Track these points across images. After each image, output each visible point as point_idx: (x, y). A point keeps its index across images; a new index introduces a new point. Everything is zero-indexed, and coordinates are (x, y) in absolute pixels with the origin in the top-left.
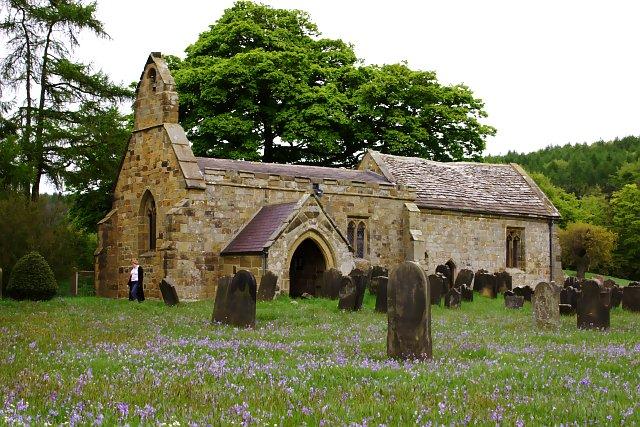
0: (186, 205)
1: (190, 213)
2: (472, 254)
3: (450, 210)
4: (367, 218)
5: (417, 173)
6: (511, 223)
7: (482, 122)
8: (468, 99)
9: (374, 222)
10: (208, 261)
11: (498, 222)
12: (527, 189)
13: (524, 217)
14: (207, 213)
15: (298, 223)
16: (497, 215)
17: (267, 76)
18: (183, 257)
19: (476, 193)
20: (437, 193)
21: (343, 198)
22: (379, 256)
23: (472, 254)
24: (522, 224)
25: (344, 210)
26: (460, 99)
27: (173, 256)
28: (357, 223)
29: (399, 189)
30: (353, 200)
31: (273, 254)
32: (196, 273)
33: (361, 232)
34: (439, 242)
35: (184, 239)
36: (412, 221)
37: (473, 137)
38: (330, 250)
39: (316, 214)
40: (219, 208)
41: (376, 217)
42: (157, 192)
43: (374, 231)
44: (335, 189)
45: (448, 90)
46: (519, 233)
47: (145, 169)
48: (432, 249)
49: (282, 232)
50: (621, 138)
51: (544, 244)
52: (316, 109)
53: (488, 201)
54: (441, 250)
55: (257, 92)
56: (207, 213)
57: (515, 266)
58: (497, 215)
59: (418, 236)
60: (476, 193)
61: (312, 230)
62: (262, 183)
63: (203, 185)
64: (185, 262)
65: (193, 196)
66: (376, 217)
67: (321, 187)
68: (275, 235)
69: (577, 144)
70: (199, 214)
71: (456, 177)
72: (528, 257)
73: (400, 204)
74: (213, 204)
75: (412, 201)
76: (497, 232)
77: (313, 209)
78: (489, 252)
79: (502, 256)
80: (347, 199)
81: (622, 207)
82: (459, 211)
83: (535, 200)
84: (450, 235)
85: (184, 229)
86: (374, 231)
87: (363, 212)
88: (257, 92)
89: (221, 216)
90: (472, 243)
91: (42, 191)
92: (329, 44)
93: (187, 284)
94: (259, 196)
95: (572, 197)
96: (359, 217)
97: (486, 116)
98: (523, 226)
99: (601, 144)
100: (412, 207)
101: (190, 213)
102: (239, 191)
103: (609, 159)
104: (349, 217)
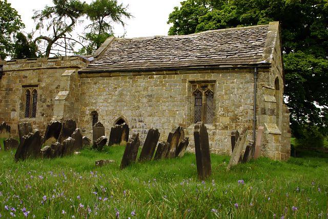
2: (145, 111)
4: (37, 86)
6: (198, 77)
9: (42, 88)
13: (214, 68)
16: (173, 70)
21: (20, 72)
22: (43, 115)
23: (145, 111)
24: (212, 77)
25: (20, 81)
29: (62, 60)
30: (27, 73)
34: (110, 101)
41: (43, 85)
43: (41, 95)
46: (213, 86)
50: (12, 6)
51: (245, 96)
54: (111, 108)
58: (173, 70)
66: (43, 85)
69: (183, 3)
72: (220, 111)
76: (179, 86)
78: (165, 108)
80: (23, 73)
84: (121, 94)
86: (41, 95)
87: (34, 81)
90: (145, 100)
98: (213, 79)
104: (23, 86)
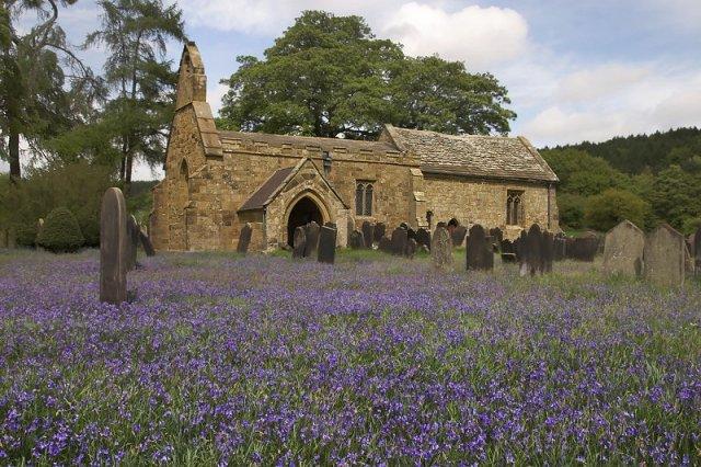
0: (205, 169)
1: (208, 177)
3: (454, 175)
5: (428, 145)
7: (504, 106)
8: (495, 87)
10: (225, 218)
11: (498, 187)
12: (531, 158)
14: (224, 177)
15: (295, 184)
17: (318, 68)
18: (203, 214)
19: (482, 161)
20: (444, 159)
26: (487, 86)
27: (193, 214)
28: (365, 186)
30: (361, 166)
31: (271, 210)
32: (215, 228)
33: (369, 193)
35: (203, 199)
36: (415, 184)
37: (501, 121)
38: (322, 201)
39: (313, 176)
40: (236, 173)
42: (189, 159)
44: (344, 157)
45: (475, 78)
47: (182, 141)
48: (436, 210)
49: (280, 192)
50: (675, 130)
52: (358, 97)
53: (492, 167)
55: (322, 76)
56: (224, 177)
57: (515, 223)
59: (420, 197)
60: (482, 161)
61: (309, 190)
62: (275, 151)
63: (220, 153)
64: (204, 218)
65: (212, 162)
67: (331, 154)
68: (274, 193)
70: (218, 177)
71: (470, 146)
73: (405, 169)
74: (230, 169)
75: (417, 167)
76: (499, 194)
77: (309, 171)
79: (503, 216)
81: (668, 183)
82: (461, 176)
83: (537, 167)
84: (454, 197)
85: (203, 190)
88: (322, 76)
89: (238, 179)
91: (134, 178)
92: (381, 43)
93: (206, 238)
94: (273, 162)
95: (626, 176)
96: (366, 181)
97: (509, 102)
99: (658, 134)
100: (416, 172)
101: (208, 177)
102: (254, 158)
103: (663, 145)
